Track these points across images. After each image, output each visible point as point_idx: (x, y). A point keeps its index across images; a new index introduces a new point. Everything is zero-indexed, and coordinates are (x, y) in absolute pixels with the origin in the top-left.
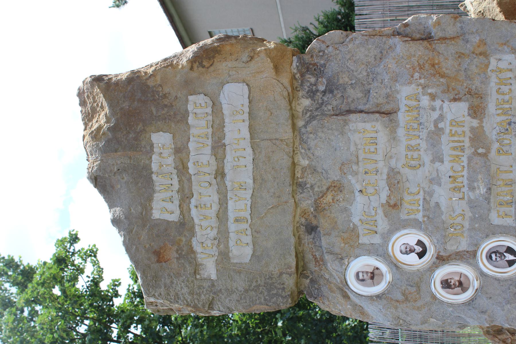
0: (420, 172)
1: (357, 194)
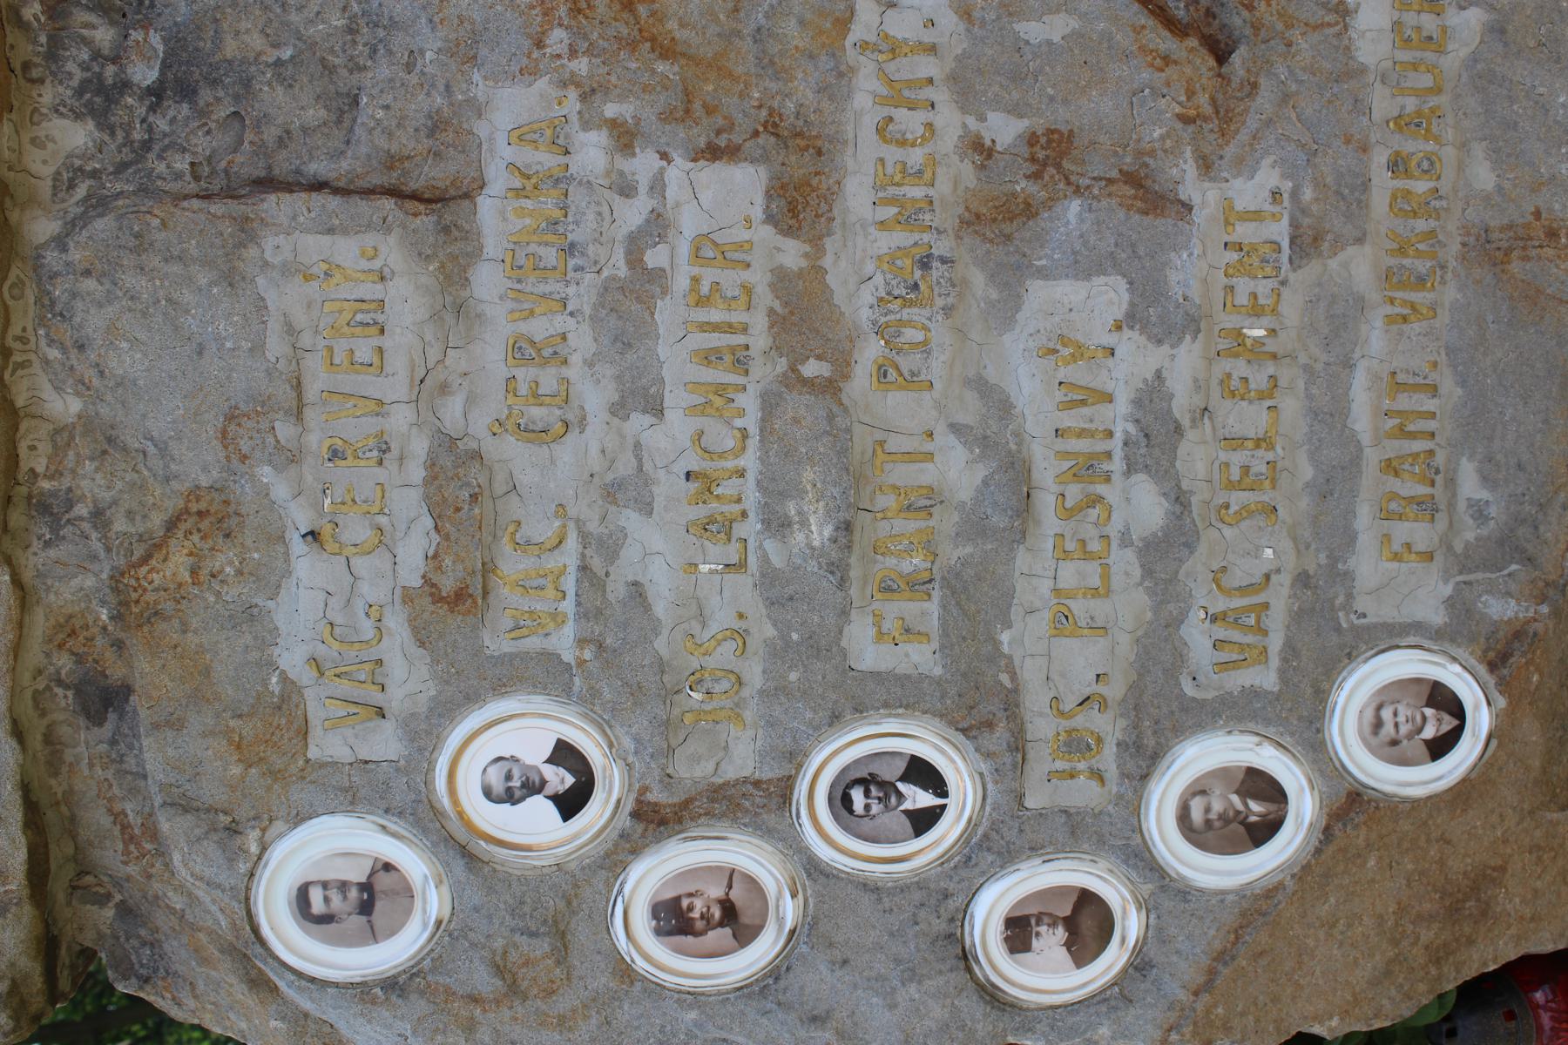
0: (566, 452)
1: (298, 546)
